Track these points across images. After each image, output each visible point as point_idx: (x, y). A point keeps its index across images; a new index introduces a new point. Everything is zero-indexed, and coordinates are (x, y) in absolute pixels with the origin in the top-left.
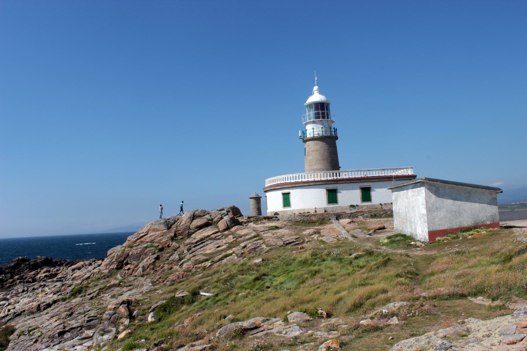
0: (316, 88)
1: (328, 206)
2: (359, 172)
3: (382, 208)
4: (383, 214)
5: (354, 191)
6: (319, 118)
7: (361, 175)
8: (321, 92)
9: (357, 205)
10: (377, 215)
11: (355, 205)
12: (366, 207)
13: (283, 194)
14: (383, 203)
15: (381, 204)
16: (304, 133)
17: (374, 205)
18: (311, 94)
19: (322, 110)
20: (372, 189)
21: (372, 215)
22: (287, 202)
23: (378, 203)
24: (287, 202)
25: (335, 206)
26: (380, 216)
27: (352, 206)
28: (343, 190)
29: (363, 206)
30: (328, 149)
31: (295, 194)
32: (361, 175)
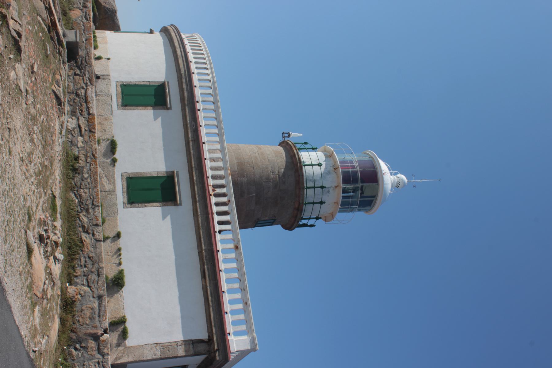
1: (113, 84)
2: (240, 306)
3: (105, 239)
4: (80, 197)
5: (161, 155)
6: (343, 192)
7: (226, 261)
8: (397, 186)
9: (114, 161)
10: (78, 178)
11: (117, 156)
12: (108, 187)
14: (121, 243)
15: (118, 235)
17: (116, 213)
18: (394, 168)
19: (360, 188)
20: (171, 208)
21: (77, 158)
23: (121, 228)
24: (135, 96)
26: (70, 186)
27: (113, 146)
28: (172, 224)
29: (112, 180)
30: (268, 179)
32: (231, 302)
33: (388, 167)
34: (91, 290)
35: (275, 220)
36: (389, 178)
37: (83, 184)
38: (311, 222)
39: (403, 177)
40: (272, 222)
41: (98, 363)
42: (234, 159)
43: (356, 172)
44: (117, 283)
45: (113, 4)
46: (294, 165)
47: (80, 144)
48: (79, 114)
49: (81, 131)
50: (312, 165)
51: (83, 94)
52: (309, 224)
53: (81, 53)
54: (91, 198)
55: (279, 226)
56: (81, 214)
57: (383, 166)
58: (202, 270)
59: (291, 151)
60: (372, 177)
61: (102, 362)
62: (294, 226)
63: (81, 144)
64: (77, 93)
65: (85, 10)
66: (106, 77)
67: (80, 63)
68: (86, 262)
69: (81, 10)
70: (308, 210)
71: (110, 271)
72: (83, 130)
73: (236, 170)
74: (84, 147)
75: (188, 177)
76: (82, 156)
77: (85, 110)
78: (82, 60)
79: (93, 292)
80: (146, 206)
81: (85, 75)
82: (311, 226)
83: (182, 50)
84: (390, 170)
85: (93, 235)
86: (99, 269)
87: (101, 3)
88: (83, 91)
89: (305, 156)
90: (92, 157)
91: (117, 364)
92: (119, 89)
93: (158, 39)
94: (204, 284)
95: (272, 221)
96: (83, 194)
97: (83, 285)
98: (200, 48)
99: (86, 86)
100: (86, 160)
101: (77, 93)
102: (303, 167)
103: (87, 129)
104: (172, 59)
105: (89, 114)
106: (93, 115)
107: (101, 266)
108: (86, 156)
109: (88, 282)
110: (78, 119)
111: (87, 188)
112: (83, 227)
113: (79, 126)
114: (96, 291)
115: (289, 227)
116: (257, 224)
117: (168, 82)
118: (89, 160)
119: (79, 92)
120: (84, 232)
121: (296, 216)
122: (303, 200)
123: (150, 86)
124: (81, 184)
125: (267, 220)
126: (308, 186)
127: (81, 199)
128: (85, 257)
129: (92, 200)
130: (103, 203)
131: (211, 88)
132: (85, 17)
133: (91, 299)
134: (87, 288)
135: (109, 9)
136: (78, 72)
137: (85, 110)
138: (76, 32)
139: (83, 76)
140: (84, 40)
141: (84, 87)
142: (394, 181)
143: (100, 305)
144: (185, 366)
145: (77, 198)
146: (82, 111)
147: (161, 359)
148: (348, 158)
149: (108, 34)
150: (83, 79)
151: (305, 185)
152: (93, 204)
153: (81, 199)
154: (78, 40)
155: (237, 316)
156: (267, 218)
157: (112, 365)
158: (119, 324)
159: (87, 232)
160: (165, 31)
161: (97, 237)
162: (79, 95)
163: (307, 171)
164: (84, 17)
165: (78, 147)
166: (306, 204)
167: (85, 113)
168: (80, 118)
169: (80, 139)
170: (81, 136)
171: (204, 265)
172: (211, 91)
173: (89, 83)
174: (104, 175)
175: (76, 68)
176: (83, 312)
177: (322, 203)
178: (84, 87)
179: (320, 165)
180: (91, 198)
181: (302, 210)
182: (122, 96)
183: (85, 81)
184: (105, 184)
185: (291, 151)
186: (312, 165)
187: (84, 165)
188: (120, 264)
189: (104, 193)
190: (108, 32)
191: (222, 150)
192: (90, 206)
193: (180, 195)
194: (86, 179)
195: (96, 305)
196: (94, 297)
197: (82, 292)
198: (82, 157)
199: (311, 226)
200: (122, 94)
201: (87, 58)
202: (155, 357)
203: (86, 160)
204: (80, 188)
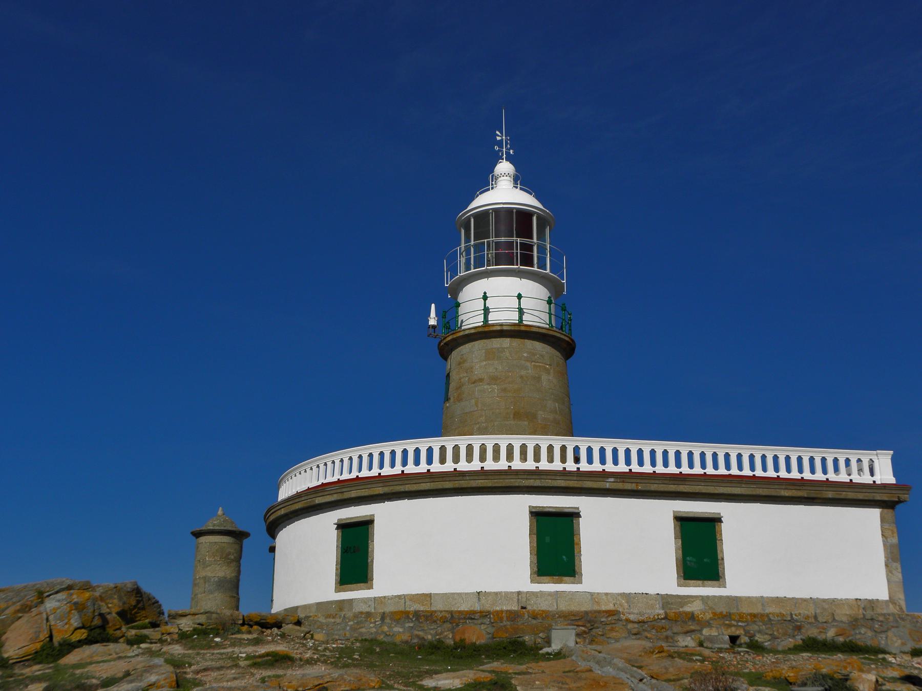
0: (504, 167)
16: (449, 311)
18: (485, 182)
31: (395, 526)
33: (481, 193)
88: (630, 626)
108: (730, 626)
122: (515, 325)
201: (574, 618)
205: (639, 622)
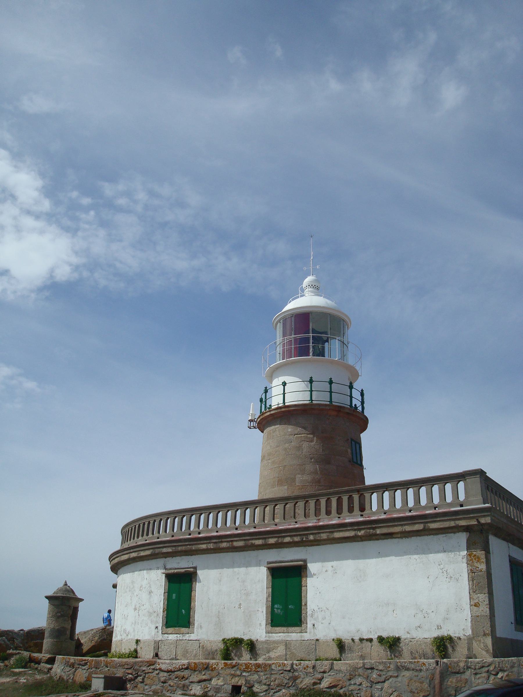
13: (171, 578)
18: (296, 293)
22: (178, 612)
24: (178, 612)
25: (293, 635)
29: (270, 646)
33: (293, 300)
34: (388, 680)
35: (352, 440)
36: (307, 300)
37: (264, 681)
38: (356, 394)
39: (309, 279)
40: (357, 445)
41: (476, 674)
42: (273, 489)
43: (295, 339)
44: (392, 644)
45: (95, 631)
46: (286, 415)
47: (220, 682)
48: (187, 681)
49: (205, 680)
50: (284, 394)
51: (166, 674)
52: (360, 398)
53: (119, 673)
54: (282, 673)
55: (362, 435)
56: (300, 686)
57: (292, 305)
58: (383, 537)
59: (269, 419)
60: (303, 319)
61: (475, 669)
62: (362, 417)
63: (219, 681)
64: (163, 682)
65: (76, 666)
66: (157, 645)
67: (130, 676)
68: (355, 684)
69: (76, 670)
70: (339, 400)
71: (377, 654)
72: (204, 677)
73: (286, 487)
74: (224, 677)
75: (367, 542)
76: (233, 680)
77: (182, 674)
78: (129, 674)
79: (391, 677)
80: (306, 605)
81: (144, 670)
82: (362, 394)
83: (132, 551)
84: (298, 297)
85: (324, 672)
86: (365, 668)
87: (93, 646)
88: (162, 674)
89: (276, 401)
90: (235, 669)
91: (493, 650)
92: (170, 630)
93: (125, 578)
94: (399, 536)
95: (353, 443)
96: (277, 682)
97: (382, 689)
98: (137, 526)
99: (157, 670)
100: (238, 676)
101: (163, 682)
102: (286, 404)
103: (204, 673)
104: (140, 564)
105: (187, 668)
106: (189, 664)
107: (362, 665)
108: (234, 676)
109: (379, 682)
110: (192, 682)
111: (270, 678)
112: (315, 684)
113: (200, 682)
114: (390, 674)
115: (362, 423)
116: (357, 463)
117: (269, 563)
118: (238, 673)
119: (162, 679)
120: (320, 683)
121: (348, 413)
122: (326, 405)
123: (273, 587)
124: (265, 684)
125: (352, 450)
126: (309, 399)
127: (282, 685)
128: (350, 684)
129: (285, 672)
130: (299, 659)
131: (307, 501)
132: (84, 666)
133: (399, 679)
134: (386, 685)
135: (100, 637)
136: (140, 679)
137: (182, 674)
138: (95, 677)
139: (146, 673)
140: (107, 669)
141: (157, 672)
142: (312, 292)
143: (408, 669)
144: (510, 561)
145: (281, 690)
146: (183, 677)
147: (491, 594)
148: (279, 349)
149: (116, 638)
150: (148, 673)
151: (328, 403)
152: (289, 671)
153: (282, 685)
154: (103, 676)
155: (335, 505)
156: (349, 450)
157: (494, 657)
158: (443, 645)
159: (321, 679)
160: (115, 569)
161: (327, 668)
162: (166, 680)
163: (291, 399)
164: (84, 668)
165: (223, 685)
166: (331, 401)
167: (186, 673)
168: (190, 681)
169: (214, 682)
170: (210, 680)
171: (376, 535)
172: (323, 502)
173: (152, 667)
174: (267, 655)
175: (136, 680)
176: (414, 690)
177: (331, 382)
178: (157, 672)
179: (284, 384)
180: (282, 673)
181: (338, 406)
182: (179, 627)
183: (150, 671)
184: (277, 654)
185: (266, 420)
186: (284, 394)
187: (244, 679)
188: (371, 640)
189: (288, 656)
190: (114, 639)
191: (316, 497)
192: (291, 674)
193: (292, 561)
194: (259, 678)
195: (407, 674)
196: (397, 676)
197: (390, 691)
198: (235, 681)
199: (362, 394)
200: (176, 627)
201: (126, 666)
202: (487, 602)
203: (238, 676)
204: (269, 685)
205: (168, 671)
